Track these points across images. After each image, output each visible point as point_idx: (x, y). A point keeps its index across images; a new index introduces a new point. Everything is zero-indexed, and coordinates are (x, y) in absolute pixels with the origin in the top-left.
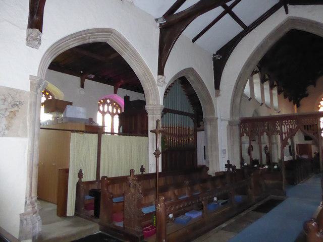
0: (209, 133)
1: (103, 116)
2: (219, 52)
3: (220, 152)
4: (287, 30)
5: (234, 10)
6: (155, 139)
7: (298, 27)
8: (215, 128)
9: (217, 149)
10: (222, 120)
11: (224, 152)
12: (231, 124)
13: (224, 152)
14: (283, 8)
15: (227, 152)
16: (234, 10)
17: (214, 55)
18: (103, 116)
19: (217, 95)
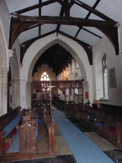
0: (16, 87)
1: (47, 78)
2: (24, 43)
3: (21, 99)
4: (55, 43)
5: (97, 8)
6: (12, 99)
7: (60, 44)
8: (19, 84)
9: (19, 97)
10: (23, 81)
11: (23, 98)
12: (28, 83)
13: (23, 98)
14: (56, 33)
15: (25, 98)
16: (97, 8)
17: (21, 44)
18: (47, 78)
19: (21, 67)
